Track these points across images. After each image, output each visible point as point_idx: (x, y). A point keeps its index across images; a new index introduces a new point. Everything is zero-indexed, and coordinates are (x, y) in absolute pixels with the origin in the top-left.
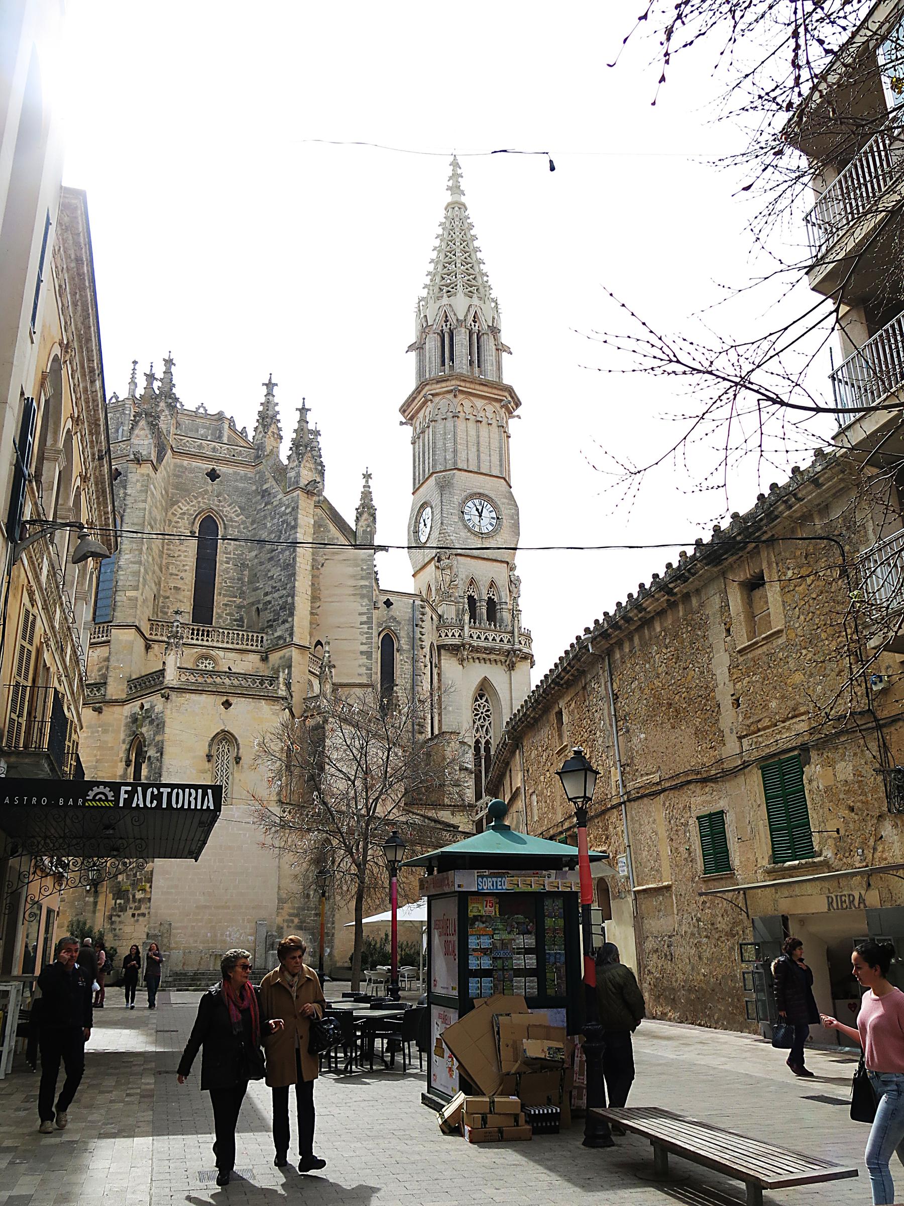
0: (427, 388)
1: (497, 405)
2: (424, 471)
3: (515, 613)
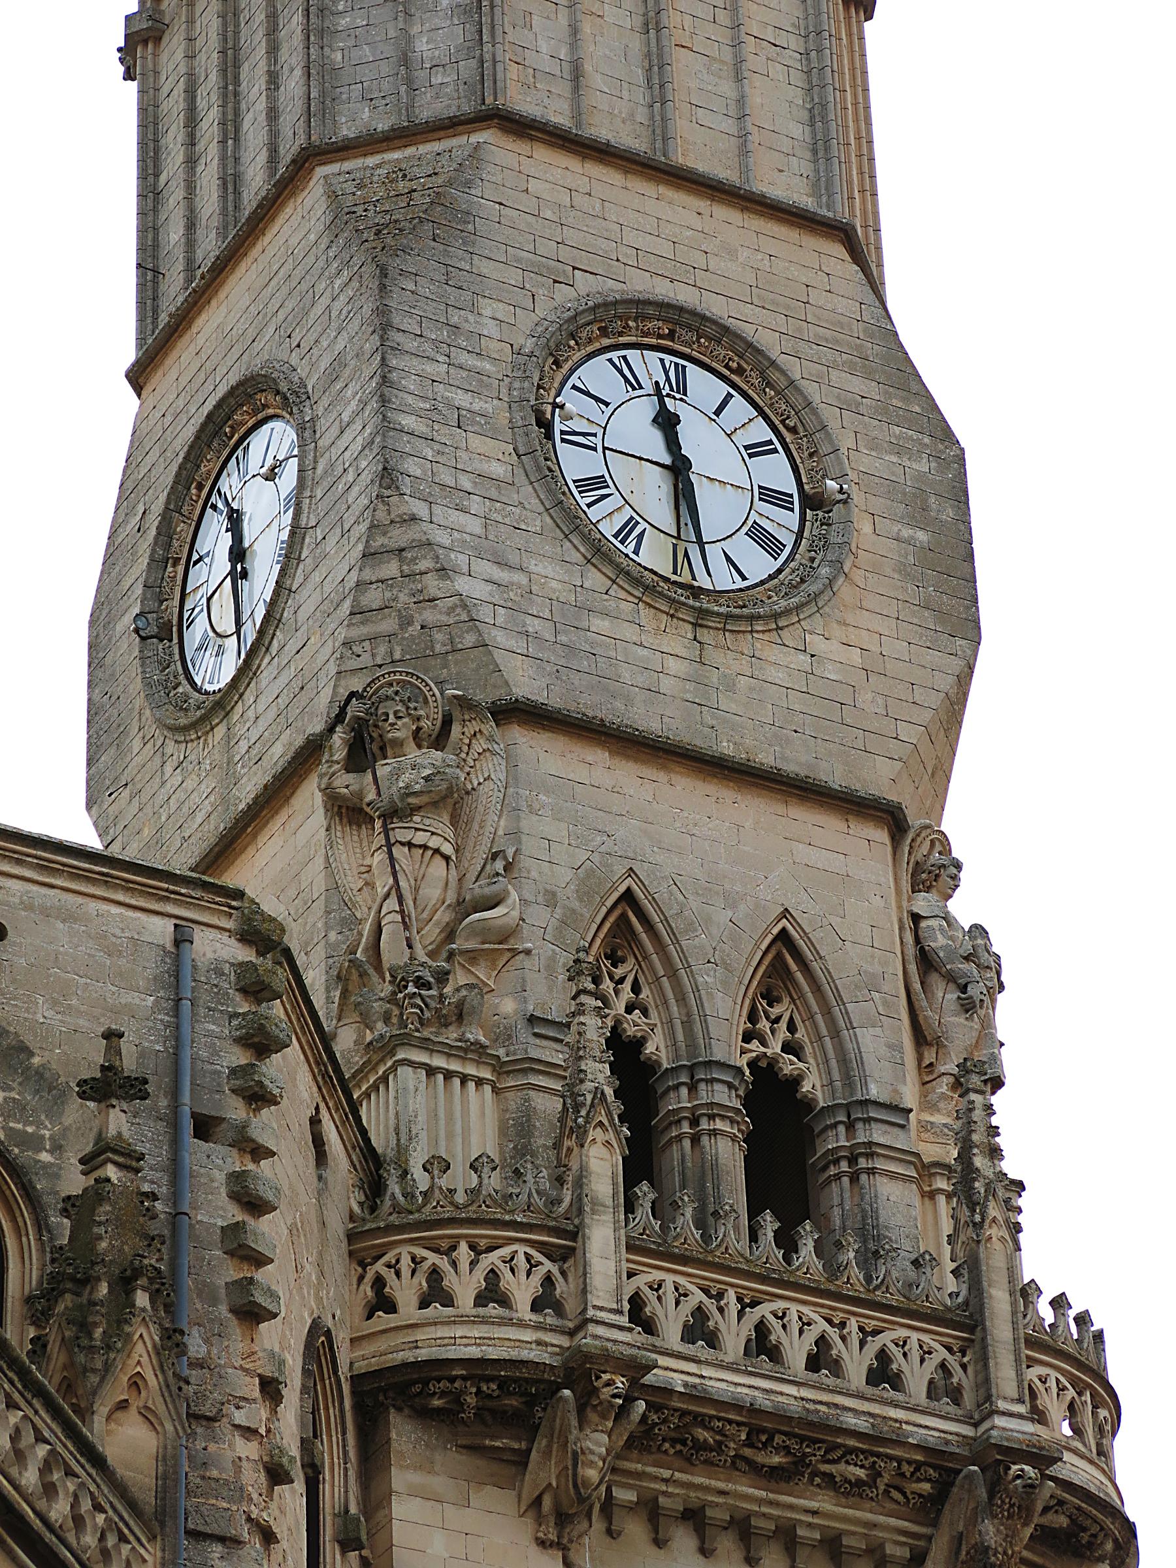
3: (980, 1192)
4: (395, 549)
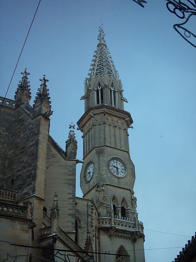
0: (91, 111)
1: (123, 121)
2: (89, 148)
4: (100, 174)
